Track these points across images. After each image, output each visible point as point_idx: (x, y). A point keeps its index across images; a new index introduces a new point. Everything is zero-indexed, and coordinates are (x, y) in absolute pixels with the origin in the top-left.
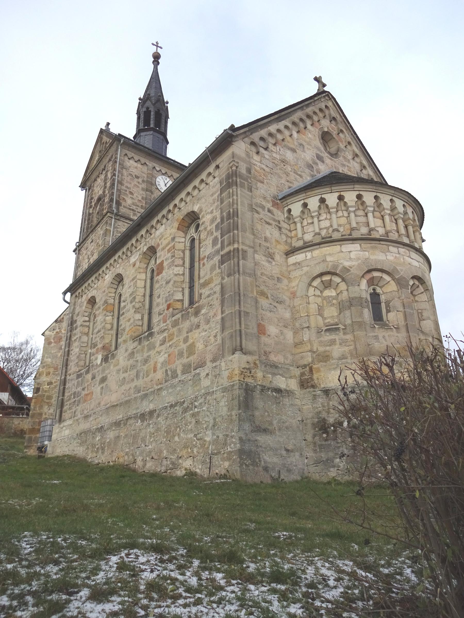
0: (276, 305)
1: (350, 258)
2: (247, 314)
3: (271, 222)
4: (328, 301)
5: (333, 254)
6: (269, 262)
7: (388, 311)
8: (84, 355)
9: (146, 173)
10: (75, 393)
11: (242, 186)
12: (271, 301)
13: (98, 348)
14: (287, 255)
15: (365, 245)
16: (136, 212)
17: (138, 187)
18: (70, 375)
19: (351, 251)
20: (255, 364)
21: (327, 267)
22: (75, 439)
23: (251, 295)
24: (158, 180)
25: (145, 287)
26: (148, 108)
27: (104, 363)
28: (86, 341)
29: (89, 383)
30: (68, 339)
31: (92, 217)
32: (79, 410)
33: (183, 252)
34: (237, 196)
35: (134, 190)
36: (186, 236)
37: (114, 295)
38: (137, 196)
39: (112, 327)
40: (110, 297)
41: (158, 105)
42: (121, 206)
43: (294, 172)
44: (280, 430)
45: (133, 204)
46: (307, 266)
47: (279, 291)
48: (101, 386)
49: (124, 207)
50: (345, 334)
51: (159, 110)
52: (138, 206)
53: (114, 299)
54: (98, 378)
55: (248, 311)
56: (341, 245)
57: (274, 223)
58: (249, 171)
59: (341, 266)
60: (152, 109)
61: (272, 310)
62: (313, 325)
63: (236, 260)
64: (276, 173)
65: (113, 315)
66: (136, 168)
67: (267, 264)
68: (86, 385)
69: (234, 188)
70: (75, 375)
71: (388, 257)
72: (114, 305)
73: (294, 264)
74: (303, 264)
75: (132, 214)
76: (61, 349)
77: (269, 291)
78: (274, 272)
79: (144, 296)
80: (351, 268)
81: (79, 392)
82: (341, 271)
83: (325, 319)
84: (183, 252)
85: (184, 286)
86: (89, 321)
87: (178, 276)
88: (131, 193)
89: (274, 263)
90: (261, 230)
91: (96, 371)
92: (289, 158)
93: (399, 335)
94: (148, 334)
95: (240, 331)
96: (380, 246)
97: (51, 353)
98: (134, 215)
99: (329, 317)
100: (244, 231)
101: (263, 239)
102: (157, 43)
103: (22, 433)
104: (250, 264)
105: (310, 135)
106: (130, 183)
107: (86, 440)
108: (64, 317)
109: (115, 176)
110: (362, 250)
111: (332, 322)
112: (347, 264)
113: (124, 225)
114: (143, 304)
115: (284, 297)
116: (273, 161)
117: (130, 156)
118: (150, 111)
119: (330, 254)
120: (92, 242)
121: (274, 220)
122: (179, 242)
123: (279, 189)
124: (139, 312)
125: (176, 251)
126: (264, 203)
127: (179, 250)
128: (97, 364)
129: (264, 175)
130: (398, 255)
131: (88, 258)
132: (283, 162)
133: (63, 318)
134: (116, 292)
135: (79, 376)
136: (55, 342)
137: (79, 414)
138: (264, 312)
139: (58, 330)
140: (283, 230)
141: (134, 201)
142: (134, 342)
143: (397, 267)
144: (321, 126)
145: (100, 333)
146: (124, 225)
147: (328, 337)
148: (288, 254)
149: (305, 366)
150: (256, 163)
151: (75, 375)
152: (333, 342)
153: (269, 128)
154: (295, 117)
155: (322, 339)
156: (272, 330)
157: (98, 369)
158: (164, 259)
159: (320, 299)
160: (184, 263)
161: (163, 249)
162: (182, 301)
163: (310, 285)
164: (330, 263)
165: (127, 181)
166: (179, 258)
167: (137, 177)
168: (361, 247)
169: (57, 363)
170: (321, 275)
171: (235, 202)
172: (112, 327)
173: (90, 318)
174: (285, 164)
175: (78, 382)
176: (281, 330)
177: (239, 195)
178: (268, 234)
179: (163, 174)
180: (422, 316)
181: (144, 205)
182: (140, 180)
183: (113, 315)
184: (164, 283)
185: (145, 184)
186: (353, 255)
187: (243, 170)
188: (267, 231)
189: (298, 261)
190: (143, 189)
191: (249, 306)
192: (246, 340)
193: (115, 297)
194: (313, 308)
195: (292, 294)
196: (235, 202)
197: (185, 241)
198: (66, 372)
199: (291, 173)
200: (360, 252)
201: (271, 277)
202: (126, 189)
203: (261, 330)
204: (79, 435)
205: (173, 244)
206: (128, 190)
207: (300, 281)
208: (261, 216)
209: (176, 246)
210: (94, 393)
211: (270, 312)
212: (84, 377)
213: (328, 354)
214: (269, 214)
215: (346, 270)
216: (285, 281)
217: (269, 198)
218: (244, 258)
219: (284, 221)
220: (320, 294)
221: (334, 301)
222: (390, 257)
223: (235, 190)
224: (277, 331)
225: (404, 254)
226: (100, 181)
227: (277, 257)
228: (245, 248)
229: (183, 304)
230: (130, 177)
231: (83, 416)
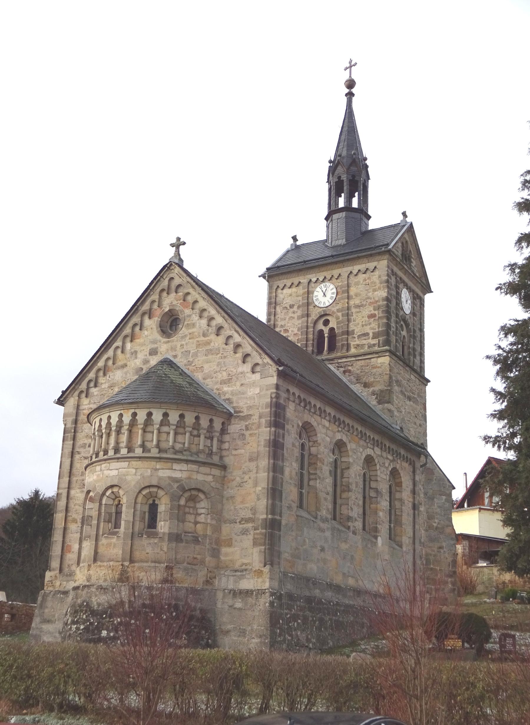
20: (56, 576)
23: (60, 527)
26: (339, 177)
44: (59, 620)
60: (344, 177)
102: (346, 69)
103: (504, 586)
154: (127, 330)
179: (323, 281)
208: (83, 454)
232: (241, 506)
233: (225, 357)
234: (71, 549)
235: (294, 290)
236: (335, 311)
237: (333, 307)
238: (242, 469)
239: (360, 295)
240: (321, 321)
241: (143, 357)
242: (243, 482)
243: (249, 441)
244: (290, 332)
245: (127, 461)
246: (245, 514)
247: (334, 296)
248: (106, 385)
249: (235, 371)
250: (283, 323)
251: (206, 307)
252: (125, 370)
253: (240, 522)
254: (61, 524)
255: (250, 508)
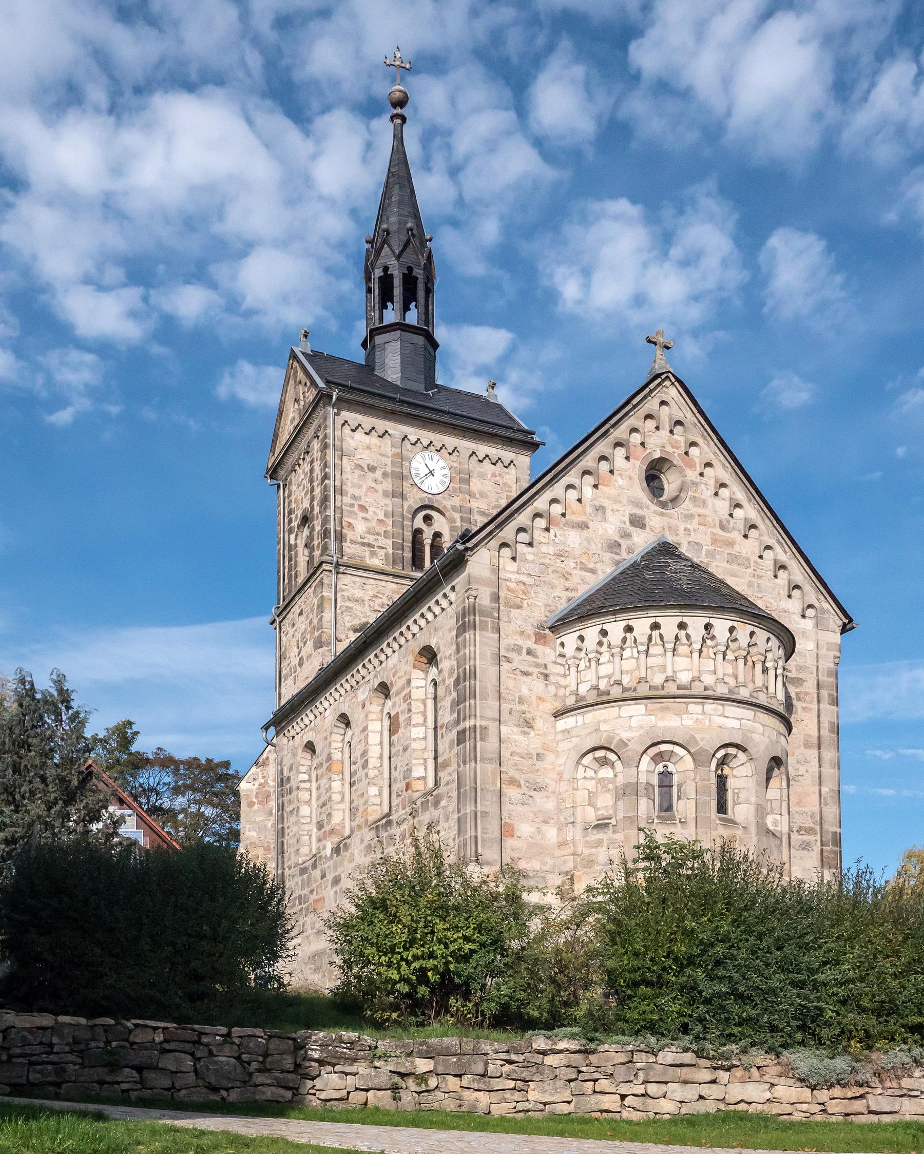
0: (532, 793)
1: (630, 727)
2: (485, 814)
3: (530, 670)
4: (603, 783)
5: (609, 720)
6: (525, 733)
7: (679, 798)
8: (308, 837)
9: (390, 454)
10: (300, 897)
11: (484, 628)
12: (524, 789)
13: (325, 832)
14: (555, 717)
15: (653, 705)
16: (376, 549)
17: (376, 491)
18: (290, 868)
19: (632, 716)
21: (600, 739)
22: (307, 964)
23: (491, 789)
24: (414, 464)
25: (381, 743)
26: (386, 269)
27: (335, 855)
28: (309, 814)
29: (318, 884)
30: (281, 809)
31: (296, 556)
32: (309, 922)
33: (424, 702)
34: (475, 646)
35: (367, 500)
36: (427, 676)
37: (341, 745)
38: (374, 513)
39: (343, 798)
40: (336, 749)
41: (409, 257)
42: (346, 542)
43: (581, 569)
45: (369, 532)
46: (577, 737)
47: (539, 773)
48: (334, 889)
49: (353, 542)
50: (614, 832)
51: (410, 269)
52: (378, 534)
53: (342, 752)
54: (330, 877)
55: (487, 810)
56: (620, 707)
57: (535, 671)
58: (496, 598)
59: (617, 738)
61: (526, 802)
62: (579, 819)
63: (472, 742)
64: (545, 582)
65: (342, 779)
66: (368, 448)
67: (520, 738)
68: (314, 886)
69: (472, 632)
70: (298, 868)
71: (684, 722)
72: (342, 762)
73: (563, 731)
74: (573, 733)
75: (367, 554)
76: (271, 814)
77: (523, 776)
78: (532, 746)
79: (381, 757)
80: (629, 740)
81: (305, 895)
82: (617, 746)
83: (598, 809)
84: (424, 702)
85: (426, 756)
86: (309, 781)
87: (418, 741)
88: (363, 508)
89: (532, 734)
90: (514, 687)
91: (326, 866)
92: (572, 545)
93: (683, 831)
94: (386, 822)
95: (476, 838)
96: (679, 704)
97: (255, 821)
98: (373, 554)
99: (603, 808)
100: (484, 698)
101: (517, 700)
104: (491, 744)
105: (620, 481)
106: (360, 487)
107: (321, 965)
108: (270, 756)
109: (329, 479)
110: (649, 713)
111: (606, 814)
112: (625, 735)
113: (354, 583)
114: (379, 771)
115: (547, 781)
116: (542, 561)
117: (354, 425)
118: (392, 275)
119: (605, 721)
120: (301, 614)
121: (537, 665)
122: (418, 688)
123: (549, 608)
124: (375, 785)
125: (412, 702)
126: (520, 642)
127: (417, 700)
128: (326, 856)
129: (524, 593)
130: (700, 717)
131: (298, 647)
132: (561, 556)
133: (267, 758)
134: (343, 740)
135: (303, 871)
136: (259, 803)
137: (309, 929)
138: (512, 807)
139: (263, 781)
140: (551, 678)
141: (369, 524)
142: (370, 829)
143: (696, 735)
144: (648, 451)
145: (325, 807)
146: (354, 583)
147: (595, 836)
148: (558, 715)
149: (567, 873)
150: (511, 576)
151: (296, 868)
152: (599, 843)
153: (535, 504)
155: (588, 838)
156: (525, 829)
157: (328, 864)
158: (399, 710)
159: (593, 782)
160: (425, 721)
161: (398, 693)
162: (424, 778)
163: (578, 763)
164: (604, 733)
165: (352, 483)
166: (418, 713)
167: (372, 469)
168: (646, 709)
169: (268, 840)
170: (595, 749)
171: (472, 655)
172: (343, 798)
173: (310, 776)
174: (563, 559)
175: (303, 880)
176: (537, 828)
177: (478, 644)
178: (525, 691)
180: (738, 797)
181: (390, 529)
182: (378, 474)
183: (342, 779)
184: (401, 748)
185: (390, 480)
186: (634, 722)
187: (485, 600)
188: (524, 686)
189: (568, 727)
190: (386, 494)
191: (489, 803)
192: (483, 847)
193: (343, 748)
194: (583, 795)
195: (558, 774)
196: (472, 655)
197: (426, 684)
198: (283, 863)
199: (574, 572)
200: (644, 717)
201: (528, 756)
202: (353, 502)
203: (506, 831)
204: (311, 958)
205: (409, 690)
206: (356, 503)
207: (568, 757)
208: (515, 665)
209: (412, 694)
210: (326, 900)
211: (523, 805)
212: (310, 873)
213: (593, 858)
214: (529, 658)
215: (623, 744)
216: (550, 757)
217: (530, 631)
218: (482, 739)
219: (555, 663)
220: (594, 775)
221: (611, 786)
222: (688, 721)
223: (472, 636)
224: (533, 829)
225: (712, 712)
226: (302, 476)
227: (539, 724)
228: (484, 723)
229: (426, 783)
230: (358, 472)
231: (315, 931)
232: (798, 809)
233: (760, 577)
234: (513, 830)
235: (373, 440)
236: (449, 507)
237: (444, 498)
238: (795, 756)
239: (487, 497)
240: (421, 515)
241: (619, 524)
242: (798, 776)
243: (803, 718)
244: (371, 513)
245: (752, 710)
246: (803, 822)
247: (447, 480)
248: (551, 550)
249: (776, 604)
250: (357, 492)
251: (727, 482)
252: (585, 533)
253: (797, 831)
254: (495, 784)
255: (810, 814)
